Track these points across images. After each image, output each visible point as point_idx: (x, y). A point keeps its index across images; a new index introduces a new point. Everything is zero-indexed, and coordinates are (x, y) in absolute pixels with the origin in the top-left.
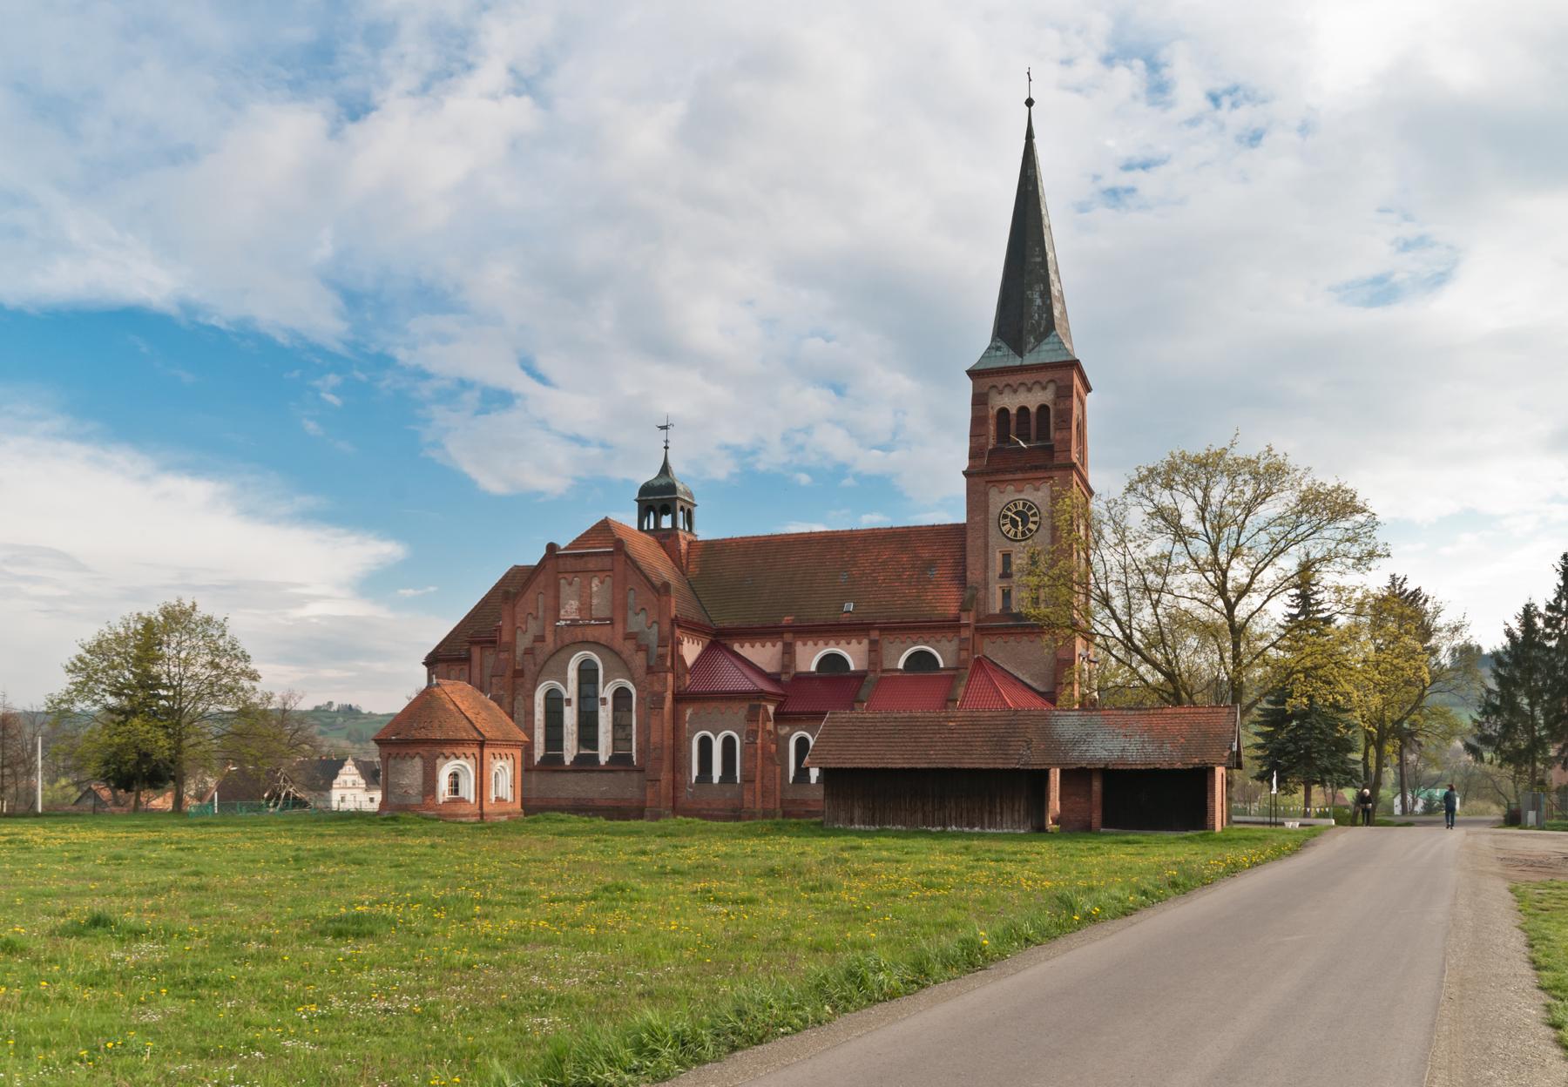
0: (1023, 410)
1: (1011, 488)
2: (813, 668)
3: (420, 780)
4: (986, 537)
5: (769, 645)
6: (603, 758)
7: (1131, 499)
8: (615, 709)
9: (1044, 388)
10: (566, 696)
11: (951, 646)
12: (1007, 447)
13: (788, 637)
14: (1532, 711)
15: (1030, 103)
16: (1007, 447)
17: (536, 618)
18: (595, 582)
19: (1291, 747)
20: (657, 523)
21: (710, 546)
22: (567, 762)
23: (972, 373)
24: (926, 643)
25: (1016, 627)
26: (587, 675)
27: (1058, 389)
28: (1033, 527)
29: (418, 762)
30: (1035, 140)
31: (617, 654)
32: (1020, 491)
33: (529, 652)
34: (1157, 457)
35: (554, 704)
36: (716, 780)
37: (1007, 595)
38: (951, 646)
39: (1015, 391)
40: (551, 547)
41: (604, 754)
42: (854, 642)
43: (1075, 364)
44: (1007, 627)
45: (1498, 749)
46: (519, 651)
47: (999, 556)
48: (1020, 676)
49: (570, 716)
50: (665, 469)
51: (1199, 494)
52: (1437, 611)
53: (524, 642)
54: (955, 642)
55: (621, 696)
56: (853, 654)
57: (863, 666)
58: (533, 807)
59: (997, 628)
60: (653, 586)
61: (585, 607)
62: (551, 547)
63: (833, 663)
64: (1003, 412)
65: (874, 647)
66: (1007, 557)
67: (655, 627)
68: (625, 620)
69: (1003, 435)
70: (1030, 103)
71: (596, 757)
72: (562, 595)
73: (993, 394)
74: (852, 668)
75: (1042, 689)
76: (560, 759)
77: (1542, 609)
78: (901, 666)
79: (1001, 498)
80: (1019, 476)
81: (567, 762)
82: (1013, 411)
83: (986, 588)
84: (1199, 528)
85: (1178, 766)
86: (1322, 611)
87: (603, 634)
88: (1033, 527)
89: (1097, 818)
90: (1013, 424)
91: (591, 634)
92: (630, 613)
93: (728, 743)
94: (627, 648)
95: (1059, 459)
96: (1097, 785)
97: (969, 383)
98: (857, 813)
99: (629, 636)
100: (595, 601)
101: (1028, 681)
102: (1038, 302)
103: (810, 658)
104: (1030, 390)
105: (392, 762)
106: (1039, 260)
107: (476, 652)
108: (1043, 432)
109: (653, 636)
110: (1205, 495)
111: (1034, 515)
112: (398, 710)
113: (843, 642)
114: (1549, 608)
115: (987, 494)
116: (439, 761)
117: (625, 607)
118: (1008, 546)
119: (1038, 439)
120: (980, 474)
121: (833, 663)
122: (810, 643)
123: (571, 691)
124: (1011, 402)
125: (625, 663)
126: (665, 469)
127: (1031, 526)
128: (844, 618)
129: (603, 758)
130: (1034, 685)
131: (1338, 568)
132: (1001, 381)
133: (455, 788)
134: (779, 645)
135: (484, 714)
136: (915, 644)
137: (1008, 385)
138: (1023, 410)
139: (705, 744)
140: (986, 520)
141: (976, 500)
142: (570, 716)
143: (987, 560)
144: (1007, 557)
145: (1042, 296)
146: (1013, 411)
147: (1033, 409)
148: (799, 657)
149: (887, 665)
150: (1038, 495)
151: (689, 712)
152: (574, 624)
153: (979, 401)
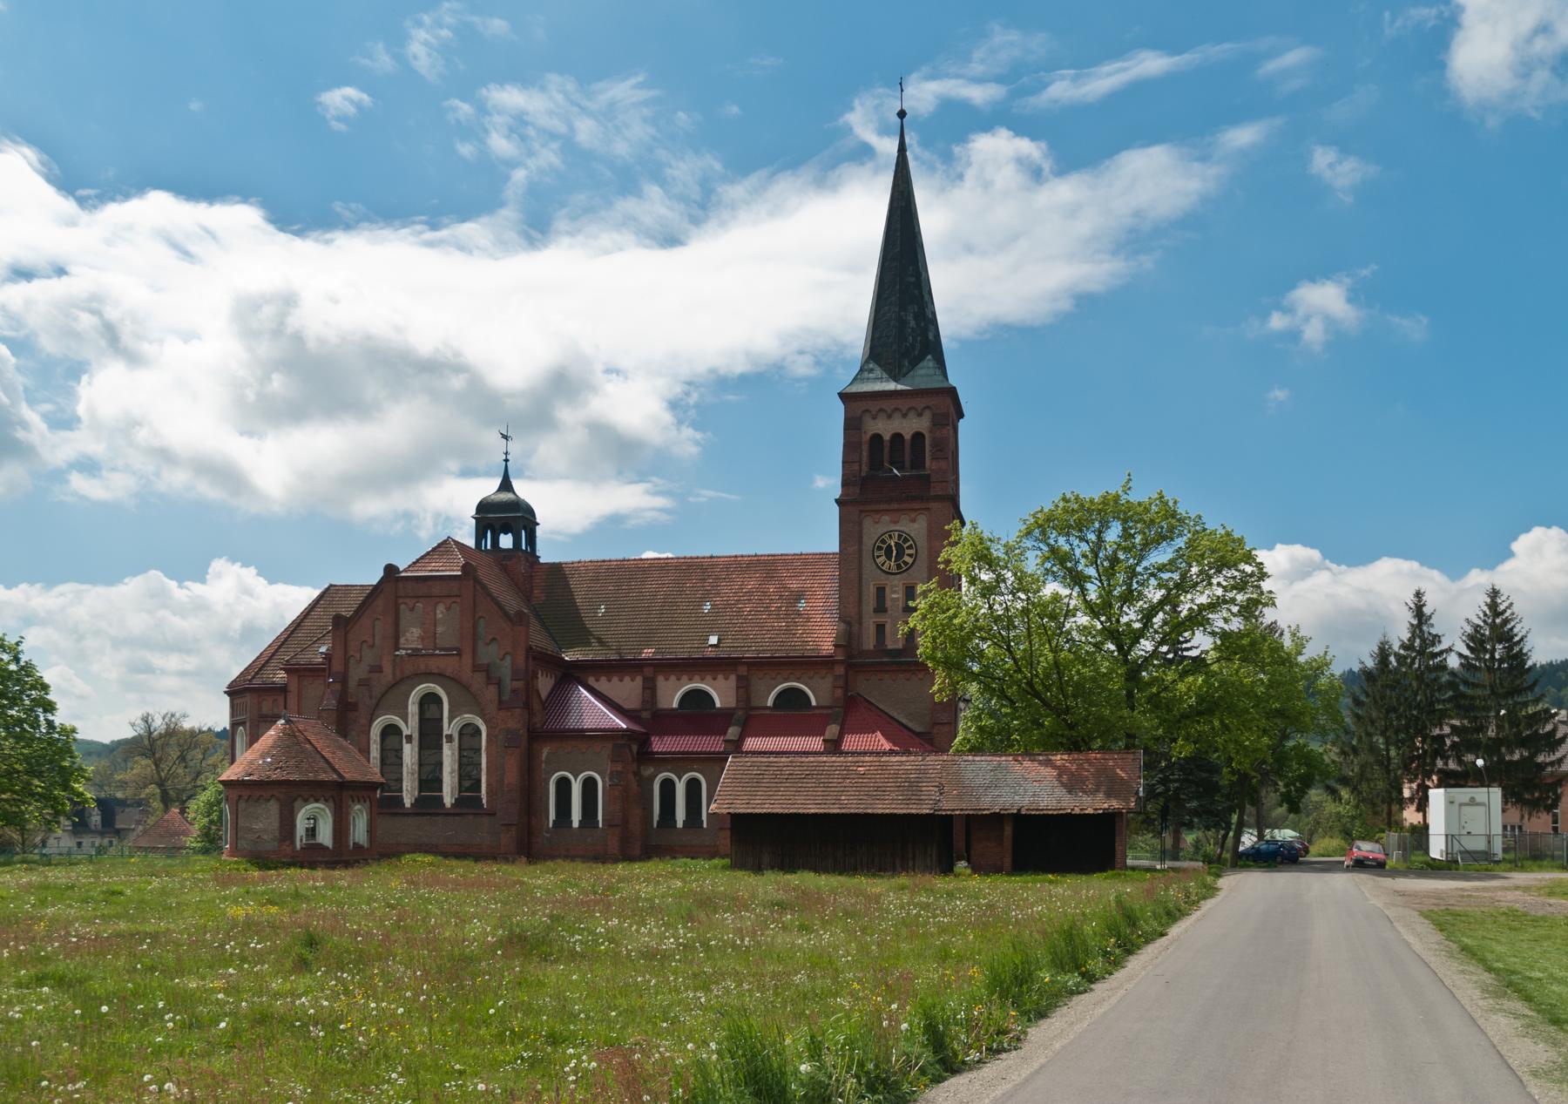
0: (897, 437)
1: (886, 518)
2: (675, 705)
3: (276, 825)
5: (627, 679)
6: (448, 800)
7: (1028, 543)
8: (422, 747)
9: (920, 415)
10: (406, 732)
11: (826, 683)
12: (880, 474)
13: (648, 672)
14: (1388, 751)
16: (880, 474)
18: (441, 609)
19: (1160, 789)
20: (495, 542)
22: (408, 805)
23: (844, 396)
24: (798, 680)
28: (909, 560)
29: (274, 807)
31: (466, 687)
32: (895, 522)
34: (1048, 501)
37: (880, 628)
38: (826, 683)
39: (889, 417)
40: (390, 570)
42: (720, 677)
43: (952, 393)
44: (882, 663)
45: (1354, 790)
46: (352, 683)
47: (872, 590)
48: (895, 715)
51: (1092, 537)
52: (1300, 644)
55: (469, 732)
59: (872, 664)
60: (506, 614)
61: (430, 635)
62: (390, 570)
63: (697, 699)
64: (877, 438)
65: (743, 686)
66: (881, 591)
67: (508, 658)
68: (474, 651)
69: (875, 463)
71: (441, 798)
72: (403, 622)
73: (867, 418)
74: (718, 705)
75: (918, 729)
77: (1396, 647)
78: (770, 703)
79: (873, 530)
81: (408, 805)
83: (860, 624)
84: (1092, 571)
85: (1090, 811)
86: (1188, 649)
87: (449, 665)
89: (1008, 861)
90: (886, 450)
91: (434, 665)
92: (480, 644)
93: (589, 785)
94: (477, 681)
95: (936, 490)
96: (1008, 830)
97: (840, 407)
98: (766, 859)
99: (487, 671)
100: (440, 629)
102: (913, 323)
103: (672, 694)
104: (905, 416)
105: (242, 805)
106: (913, 279)
108: (918, 461)
109: (505, 669)
110: (1099, 537)
111: (910, 547)
112: (107, 741)
113: (709, 678)
114: (1403, 646)
115: (860, 524)
116: (297, 804)
117: (475, 637)
118: (883, 580)
119: (912, 467)
122: (673, 678)
123: (410, 727)
124: (885, 428)
128: (710, 653)
129: (448, 800)
130: (910, 725)
131: (1225, 614)
132: (874, 406)
133: (312, 832)
134: (639, 680)
135: (340, 753)
136: (786, 680)
137: (881, 410)
138: (897, 437)
139: (564, 787)
140: (860, 551)
141: (850, 530)
142: (409, 753)
143: (860, 593)
145: (916, 317)
146: (887, 437)
147: (907, 437)
148: (660, 692)
150: (916, 527)
151: (545, 751)
152: (415, 653)
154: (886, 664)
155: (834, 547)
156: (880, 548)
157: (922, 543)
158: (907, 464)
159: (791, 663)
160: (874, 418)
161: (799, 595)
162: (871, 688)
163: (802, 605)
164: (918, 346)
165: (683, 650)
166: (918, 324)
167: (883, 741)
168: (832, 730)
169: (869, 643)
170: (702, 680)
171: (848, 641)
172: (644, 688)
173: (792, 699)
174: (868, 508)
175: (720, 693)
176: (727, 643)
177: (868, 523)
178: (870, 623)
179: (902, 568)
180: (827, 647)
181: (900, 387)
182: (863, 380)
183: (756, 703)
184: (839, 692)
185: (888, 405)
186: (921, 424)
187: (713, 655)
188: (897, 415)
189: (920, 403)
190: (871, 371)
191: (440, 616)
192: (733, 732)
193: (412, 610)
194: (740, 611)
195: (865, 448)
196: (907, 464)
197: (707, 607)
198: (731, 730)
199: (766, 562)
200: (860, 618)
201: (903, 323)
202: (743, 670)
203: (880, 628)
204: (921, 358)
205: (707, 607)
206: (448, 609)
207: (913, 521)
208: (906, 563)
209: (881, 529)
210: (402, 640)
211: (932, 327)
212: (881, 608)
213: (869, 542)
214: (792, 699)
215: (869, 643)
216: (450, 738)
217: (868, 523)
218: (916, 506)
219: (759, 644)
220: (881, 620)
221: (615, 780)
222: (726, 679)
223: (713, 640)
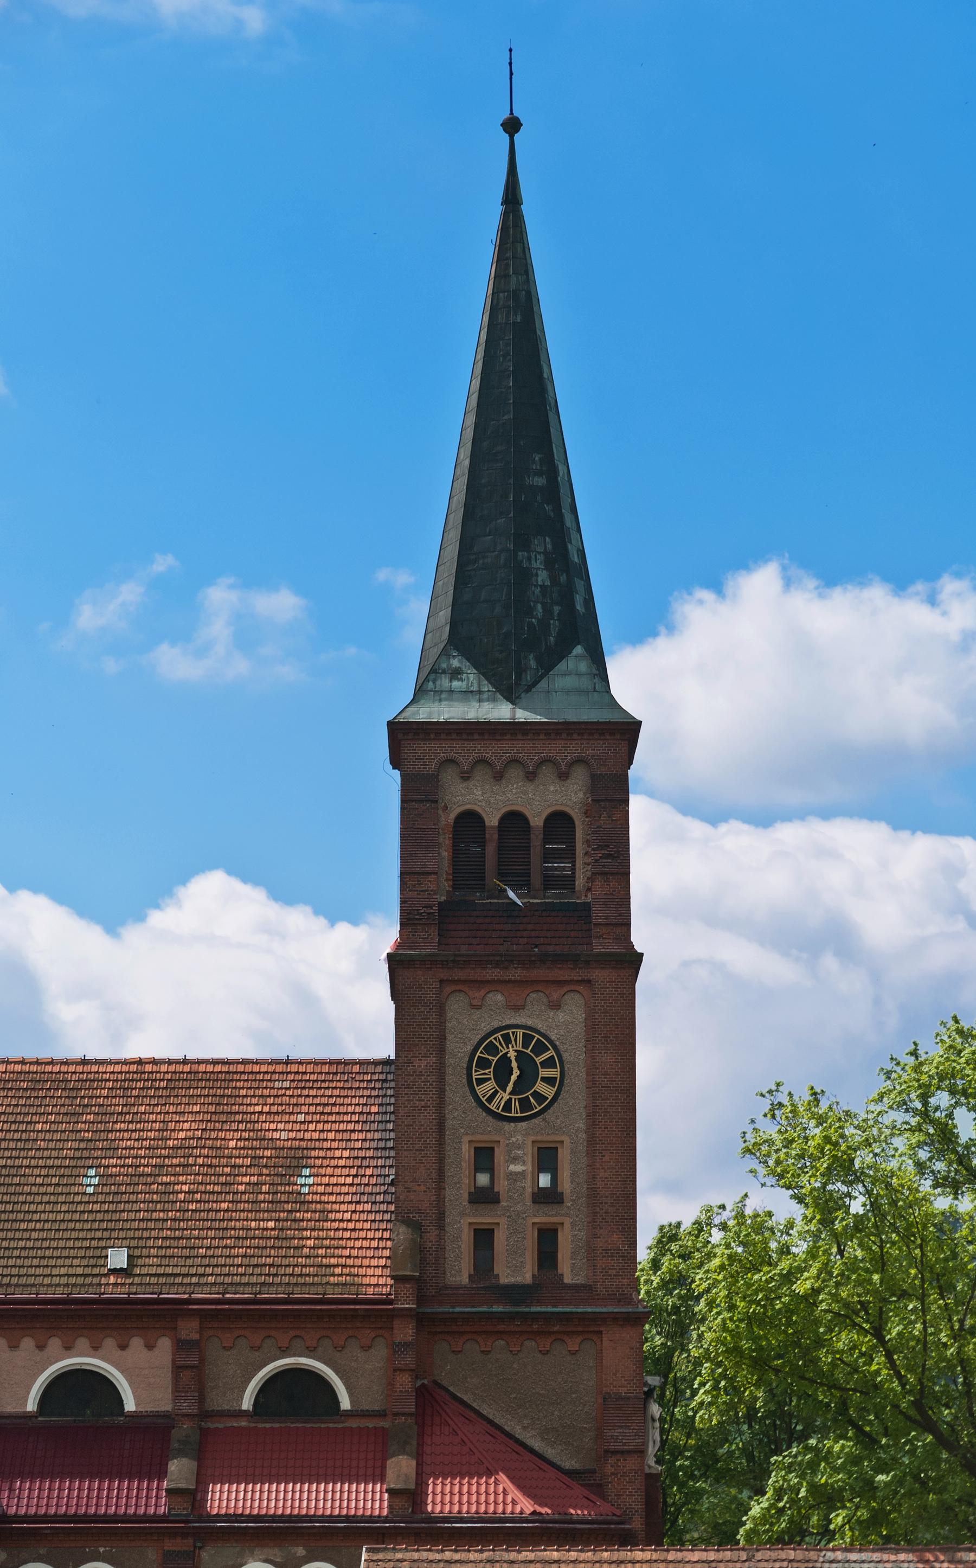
0: (514, 821)
2: (31, 1406)
4: (441, 1104)
9: (563, 776)
11: (375, 1359)
12: (478, 898)
15: (512, 126)
24: (310, 1352)
25: (512, 1317)
27: (595, 779)
28: (548, 1091)
30: (525, 208)
32: (517, 1008)
37: (484, 1237)
38: (375, 1359)
39: (499, 776)
42: (137, 1343)
44: (490, 1316)
48: (518, 1432)
54: (380, 1353)
57: (163, 1402)
58: (649, 1476)
64: (470, 821)
65: (190, 1372)
66: (484, 1157)
69: (467, 873)
70: (512, 126)
73: (449, 777)
74: (130, 1405)
75: (568, 1464)
78: (247, 1403)
79: (470, 1022)
80: (516, 973)
82: (492, 820)
83: (441, 1227)
88: (548, 1091)
90: (491, 849)
101: (536, 1444)
102: (543, 577)
104: (531, 776)
111: (549, 1063)
113: (110, 1343)
115: (441, 1010)
118: (489, 1131)
120: (429, 962)
122: (28, 1343)
124: (489, 800)
127: (541, 1087)
128: (114, 1289)
130: (550, 1453)
132: (466, 752)
136: (285, 1352)
138: (514, 821)
140: (441, 1069)
143: (441, 1160)
146: (492, 820)
153: (418, 797)
154: (501, 1317)
155: (385, 1048)
156: (484, 1064)
157: (575, 1054)
158: (536, 880)
159: (262, 1315)
160: (466, 777)
161: (294, 1159)
162: (469, 1372)
163: (305, 1181)
164: (555, 626)
165: (55, 1280)
166: (553, 578)
167: (514, 1493)
168: (401, 1468)
169: (460, 1270)
170: (95, 1348)
171: (419, 1267)
172: (177, 1369)
173: (296, 1396)
174: (458, 974)
175: (135, 1380)
176: (150, 1266)
177: (456, 1007)
178: (461, 1224)
179: (530, 1108)
180: (376, 1279)
181: (522, 715)
182: (439, 695)
183: (217, 1402)
184: (405, 1382)
185: (494, 751)
186: (570, 796)
187: (120, 1293)
188: (514, 773)
189: (564, 750)
190: (456, 674)
192: (179, 1470)
194: (167, 1191)
195: (446, 840)
196: (536, 880)
197: (91, 1180)
198: (174, 1466)
199: (212, 1078)
200: (441, 1215)
201: (524, 576)
202: (189, 1329)
203: (484, 1237)
204: (561, 652)
205: (91, 1180)
207: (556, 1006)
208: (540, 1097)
209: (485, 1028)
213: (459, 1050)
214: (296, 1396)
215: (460, 1270)
217: (456, 1007)
218: (563, 975)
219: (221, 1268)
220: (484, 1219)
222: (150, 1347)
223: (118, 1258)
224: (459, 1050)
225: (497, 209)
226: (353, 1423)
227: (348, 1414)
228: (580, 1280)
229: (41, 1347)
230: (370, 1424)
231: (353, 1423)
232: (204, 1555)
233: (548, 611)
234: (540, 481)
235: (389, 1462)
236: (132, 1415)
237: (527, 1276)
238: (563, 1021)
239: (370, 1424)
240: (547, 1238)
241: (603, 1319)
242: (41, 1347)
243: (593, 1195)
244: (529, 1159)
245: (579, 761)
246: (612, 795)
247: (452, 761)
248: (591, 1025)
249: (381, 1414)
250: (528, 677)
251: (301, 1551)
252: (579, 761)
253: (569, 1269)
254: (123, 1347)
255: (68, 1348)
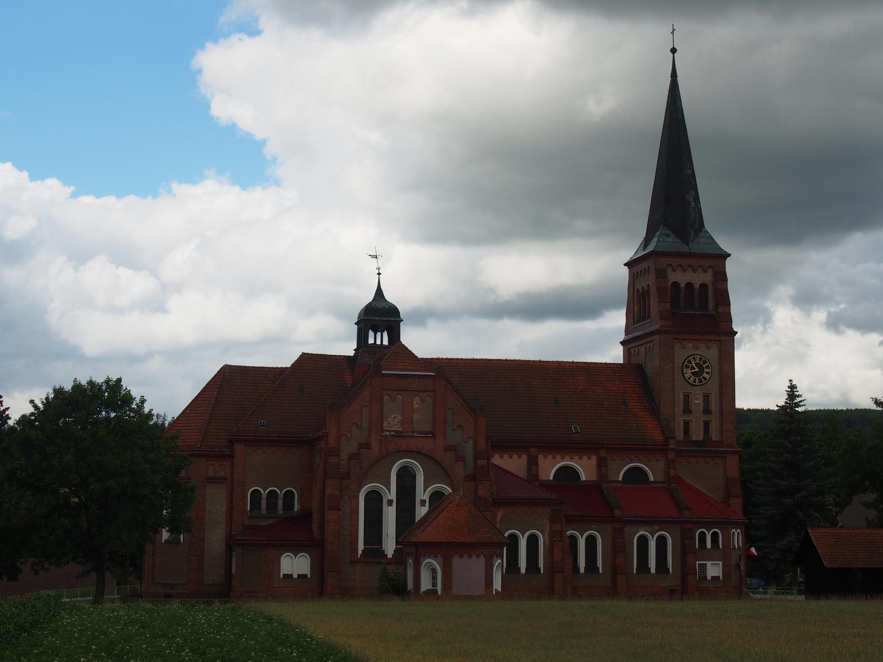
0: (689, 285)
2: (551, 478)
5: (515, 456)
9: (705, 271)
15: (674, 51)
17: (360, 428)
18: (416, 401)
21: (792, 424)
22: (390, 556)
24: (640, 461)
26: (406, 480)
29: (482, 561)
32: (697, 348)
33: (352, 457)
35: (375, 501)
36: (653, 570)
37: (687, 424)
39: (684, 271)
41: (709, 545)
46: (344, 455)
49: (390, 515)
50: (379, 293)
53: (348, 448)
56: (585, 469)
57: (594, 477)
63: (566, 473)
64: (675, 284)
65: (601, 464)
66: (687, 396)
70: (674, 51)
74: (583, 478)
76: (383, 554)
78: (620, 479)
81: (390, 556)
93: (532, 542)
99: (449, 448)
100: (416, 417)
102: (693, 204)
103: (550, 468)
104: (684, 271)
107: (239, 449)
111: (708, 367)
113: (576, 457)
116: (495, 558)
121: (566, 473)
125: (446, 471)
126: (379, 293)
127: (705, 375)
134: (524, 457)
136: (632, 462)
138: (689, 285)
142: (390, 515)
144: (687, 396)
145: (695, 201)
146: (683, 285)
147: (697, 286)
149: (611, 478)
151: (500, 514)
152: (398, 435)
169: (697, 435)
183: (611, 478)
186: (707, 278)
190: (668, 236)
191: (416, 406)
193: (393, 400)
203: (687, 424)
206: (423, 401)
207: (708, 348)
210: (385, 424)
211: (692, 193)
212: (687, 410)
213: (679, 362)
216: (423, 503)
221: (554, 537)
222: (589, 459)
224: (679, 362)
225: (668, 80)
226: (655, 485)
227: (651, 482)
228: (718, 439)
229: (554, 458)
230: (660, 485)
231: (655, 485)
232: (626, 529)
233: (695, 216)
234: (690, 172)
235: (855, 498)
236: (583, 481)
237: (701, 437)
238: (711, 353)
239: (660, 485)
240: (707, 424)
241: (725, 452)
242: (554, 458)
243: (721, 411)
244: (701, 399)
245: (710, 267)
246: (721, 277)
247: (670, 265)
248: (720, 355)
249: (663, 482)
250: (692, 238)
251: (656, 528)
252: (710, 267)
253: (715, 436)
254: (581, 459)
255: (563, 459)
